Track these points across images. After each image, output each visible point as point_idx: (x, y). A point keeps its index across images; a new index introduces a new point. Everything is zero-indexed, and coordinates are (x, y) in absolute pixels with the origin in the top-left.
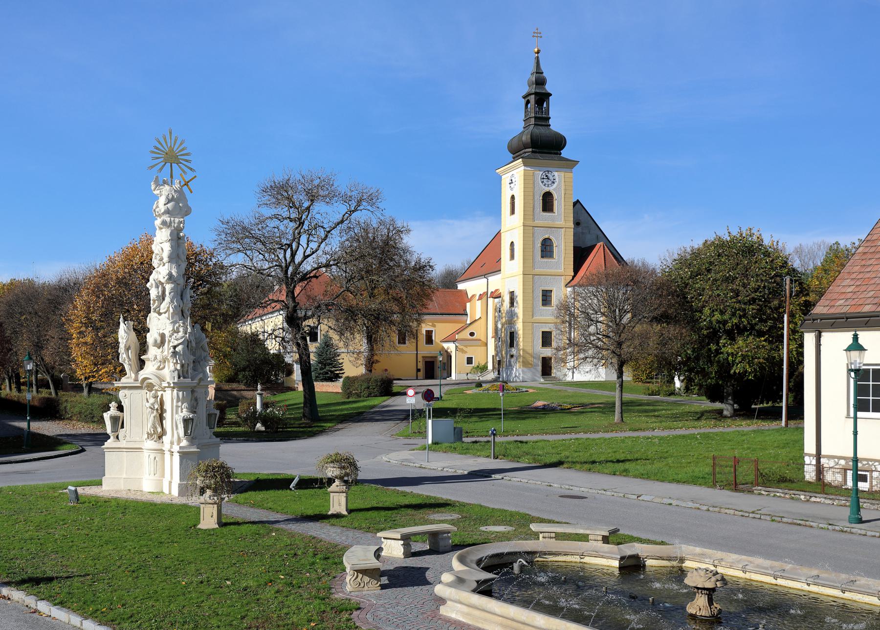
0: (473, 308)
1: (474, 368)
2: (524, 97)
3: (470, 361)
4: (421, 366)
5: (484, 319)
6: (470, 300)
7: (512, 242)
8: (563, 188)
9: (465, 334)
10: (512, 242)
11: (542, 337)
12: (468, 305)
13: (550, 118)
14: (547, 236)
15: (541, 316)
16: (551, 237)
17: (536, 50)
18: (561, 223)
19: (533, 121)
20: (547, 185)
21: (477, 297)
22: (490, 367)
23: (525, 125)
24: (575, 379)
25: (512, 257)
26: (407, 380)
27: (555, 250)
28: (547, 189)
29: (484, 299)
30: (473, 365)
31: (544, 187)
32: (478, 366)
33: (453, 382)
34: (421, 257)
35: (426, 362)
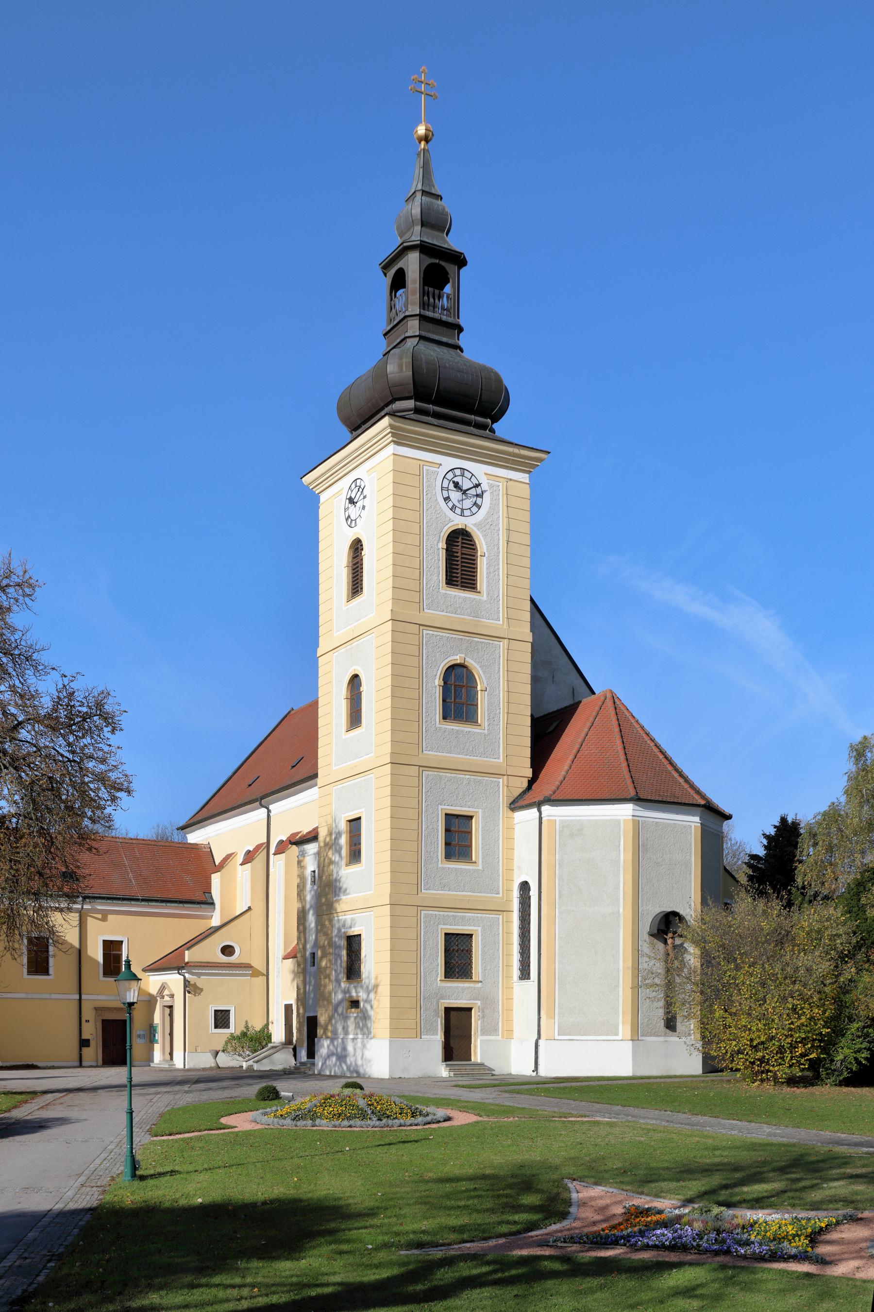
0: (228, 888)
1: (233, 1037)
2: (386, 267)
3: (222, 1019)
4: (91, 1031)
5: (258, 910)
6: (218, 868)
7: (355, 677)
8: (502, 524)
9: (210, 951)
10: (355, 677)
11: (446, 950)
12: (216, 879)
13: (460, 261)
14: (458, 659)
15: (443, 887)
16: (471, 662)
17: (421, 130)
18: (498, 623)
19: (413, 327)
20: (458, 511)
21: (240, 858)
22: (278, 1034)
23: (388, 345)
24: (549, 1069)
25: (355, 718)
26: (53, 1068)
27: (482, 700)
28: (458, 522)
29: (261, 857)
30: (232, 1029)
31: (450, 514)
32: (244, 1034)
33: (179, 1076)
34: (75, 685)
35: (104, 1022)
